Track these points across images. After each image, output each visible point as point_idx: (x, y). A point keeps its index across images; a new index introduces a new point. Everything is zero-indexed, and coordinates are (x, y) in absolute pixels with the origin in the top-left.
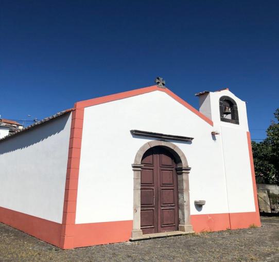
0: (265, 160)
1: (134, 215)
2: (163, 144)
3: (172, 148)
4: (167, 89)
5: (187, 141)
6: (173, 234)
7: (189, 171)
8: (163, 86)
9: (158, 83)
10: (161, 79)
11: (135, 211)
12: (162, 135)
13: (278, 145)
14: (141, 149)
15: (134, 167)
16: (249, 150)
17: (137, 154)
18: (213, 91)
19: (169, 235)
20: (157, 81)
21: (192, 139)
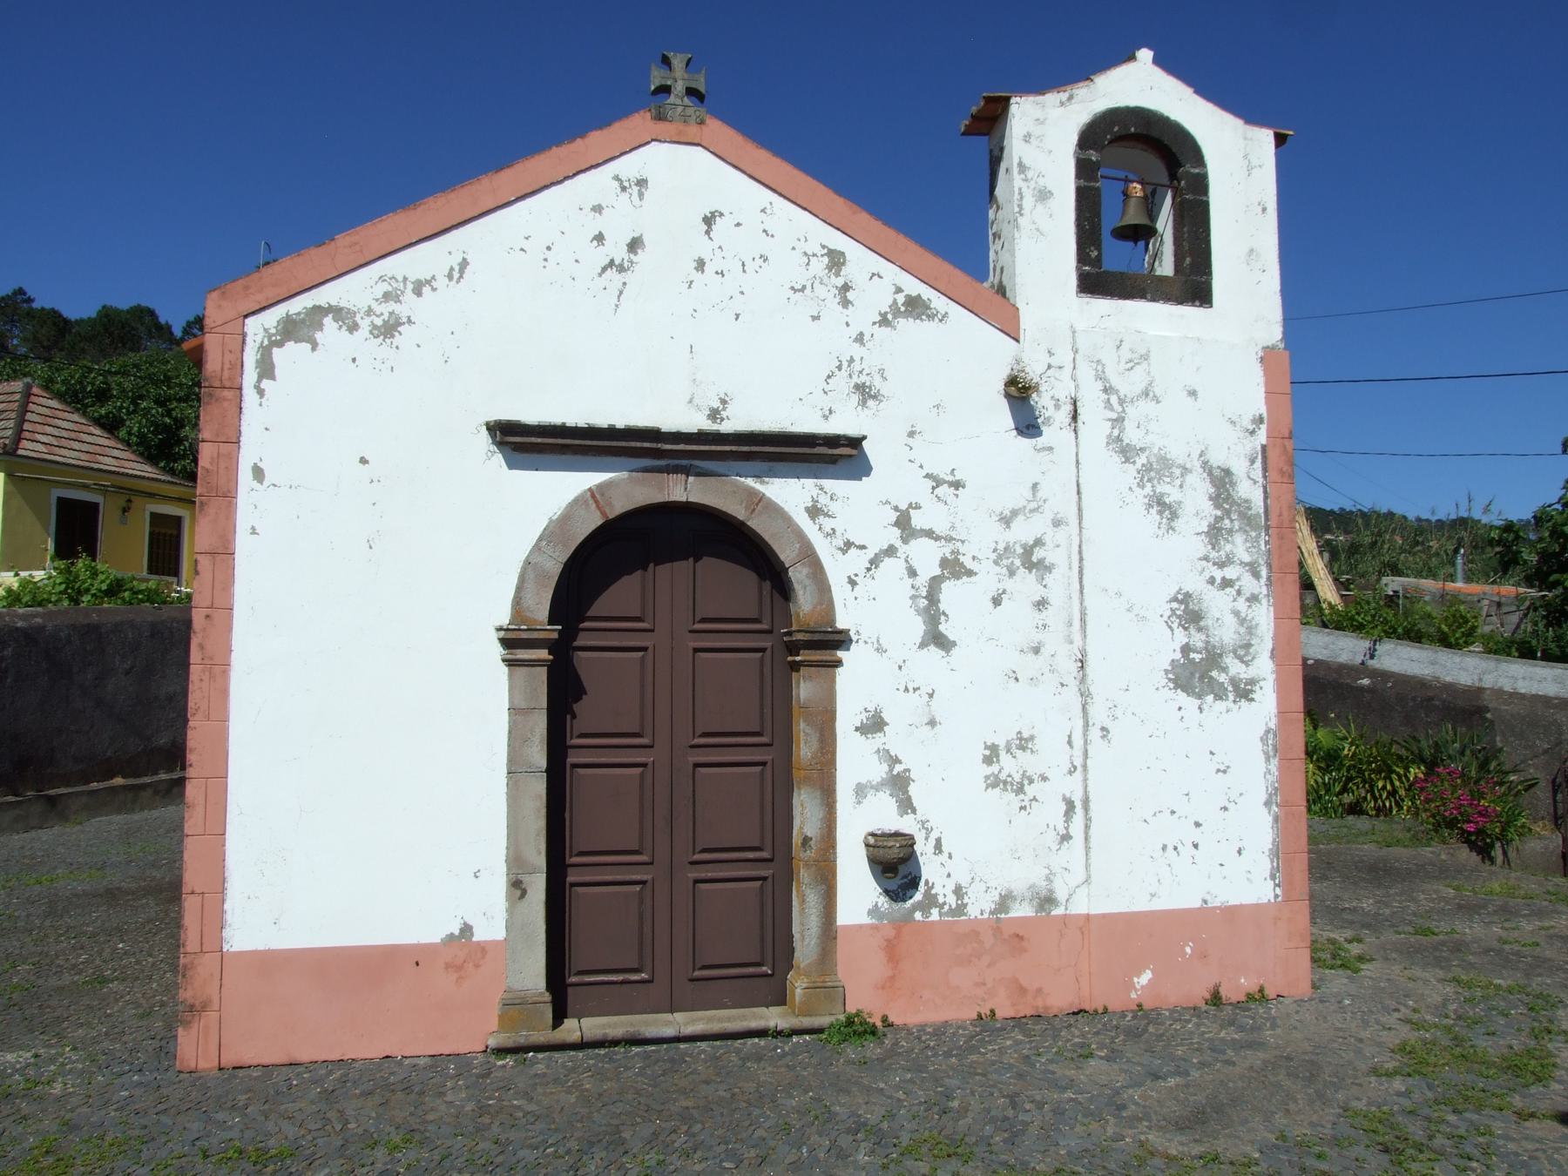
0: (881, 1060)
1: (511, 911)
2: (681, 490)
3: (738, 511)
4: (715, 127)
5: (833, 460)
6: (716, 1027)
7: (840, 654)
8: (694, 110)
9: (664, 90)
10: (678, 62)
11: (517, 887)
12: (654, 434)
13: (958, 1175)
14: (554, 532)
15: (507, 643)
16: (221, 775)
17: (527, 562)
18: (1038, 87)
19: (689, 1030)
20: (657, 77)
21: (864, 438)
